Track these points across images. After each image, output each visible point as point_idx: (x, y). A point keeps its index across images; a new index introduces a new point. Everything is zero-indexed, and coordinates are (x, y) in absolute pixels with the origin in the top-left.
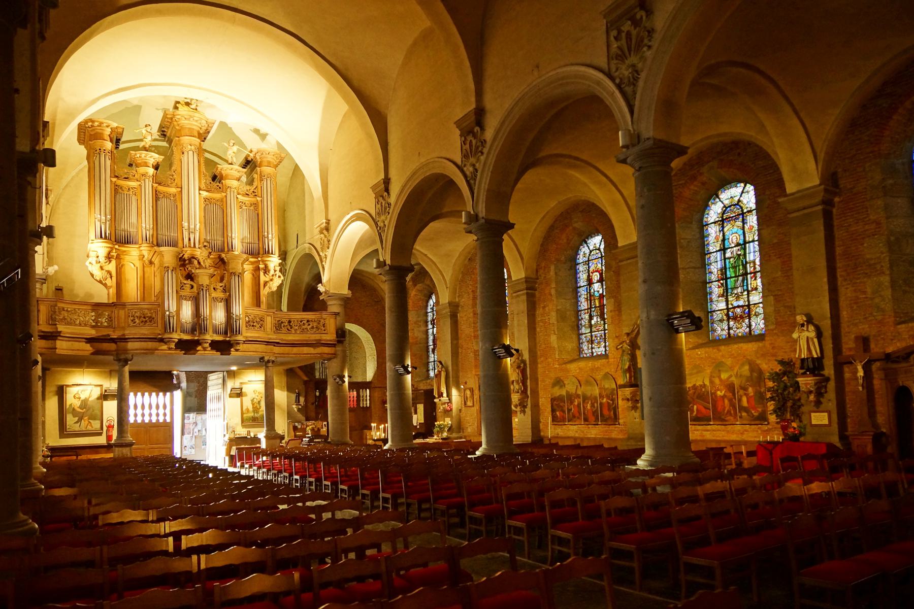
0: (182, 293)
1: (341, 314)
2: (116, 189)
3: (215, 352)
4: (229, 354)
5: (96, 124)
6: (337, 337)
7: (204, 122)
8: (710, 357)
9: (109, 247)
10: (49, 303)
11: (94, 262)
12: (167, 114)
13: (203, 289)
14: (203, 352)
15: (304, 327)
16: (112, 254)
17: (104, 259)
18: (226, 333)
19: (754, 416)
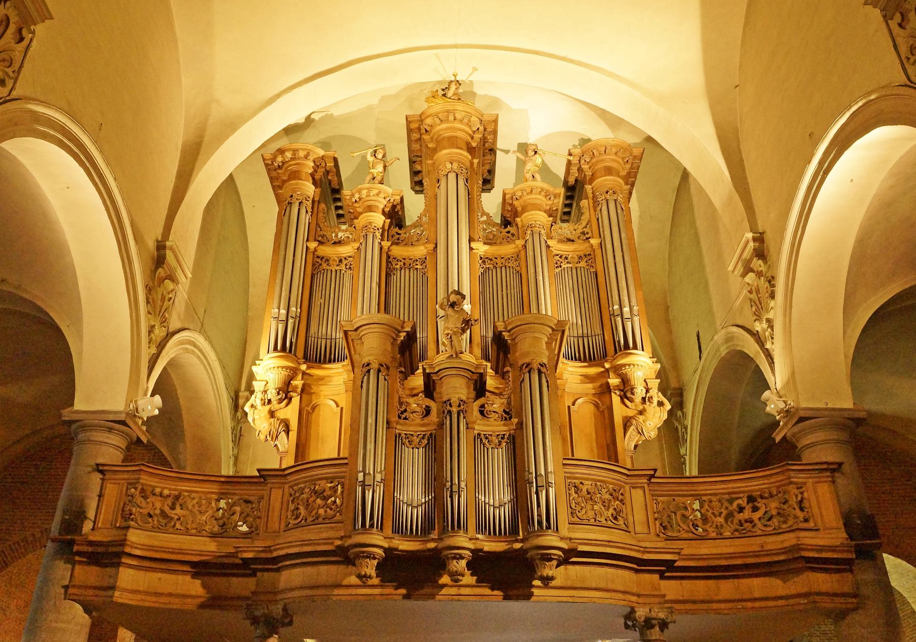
0: (401, 429)
1: (846, 468)
2: (317, 265)
3: (487, 591)
4: (528, 596)
5: (289, 155)
6: (851, 537)
7: (476, 124)
9: (287, 368)
10: (126, 476)
11: (258, 403)
12: (410, 122)
13: (450, 412)
14: (454, 591)
15: (741, 516)
16: (294, 383)
17: (274, 392)
18: (514, 531)
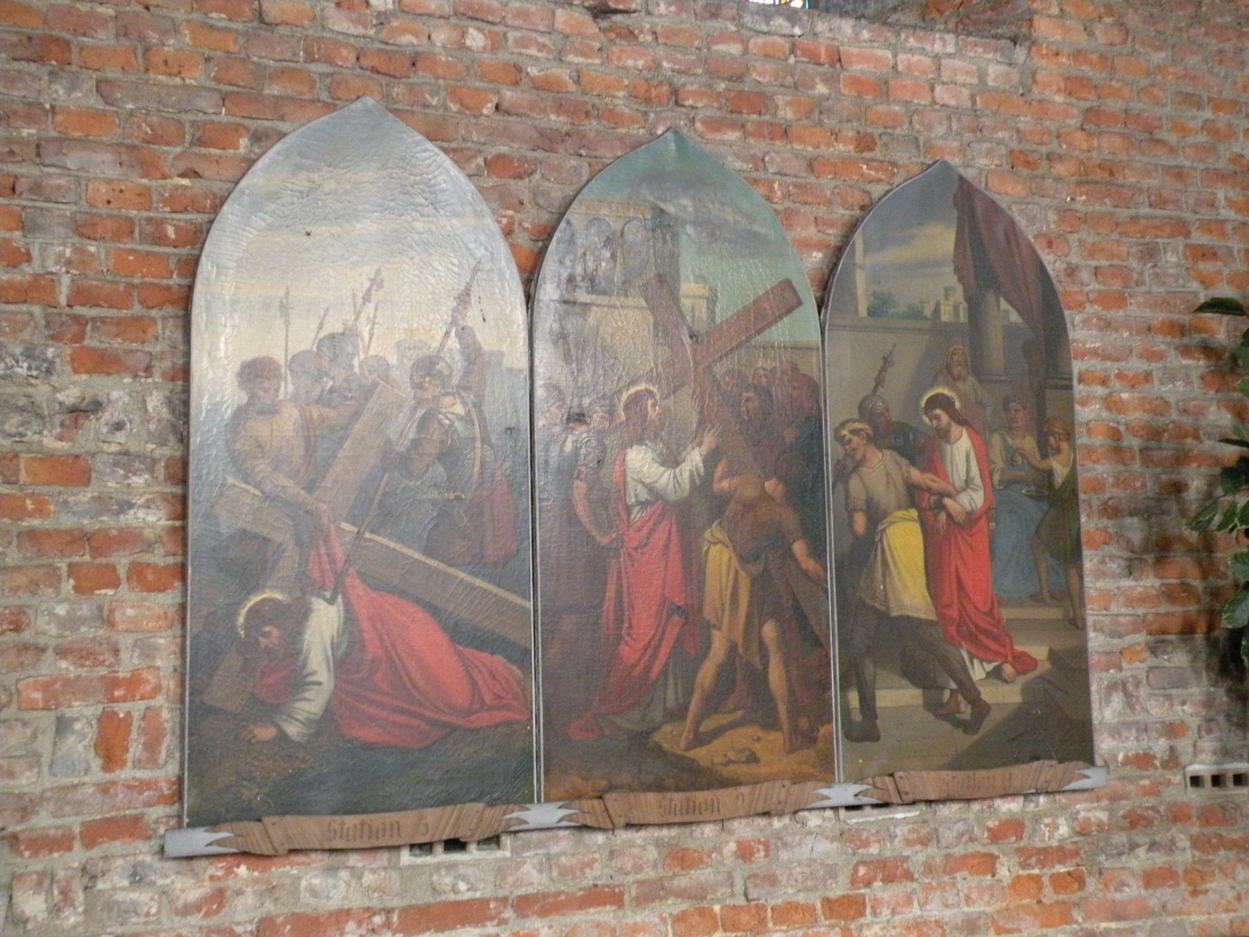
8: (515, 75)
19: (981, 709)
